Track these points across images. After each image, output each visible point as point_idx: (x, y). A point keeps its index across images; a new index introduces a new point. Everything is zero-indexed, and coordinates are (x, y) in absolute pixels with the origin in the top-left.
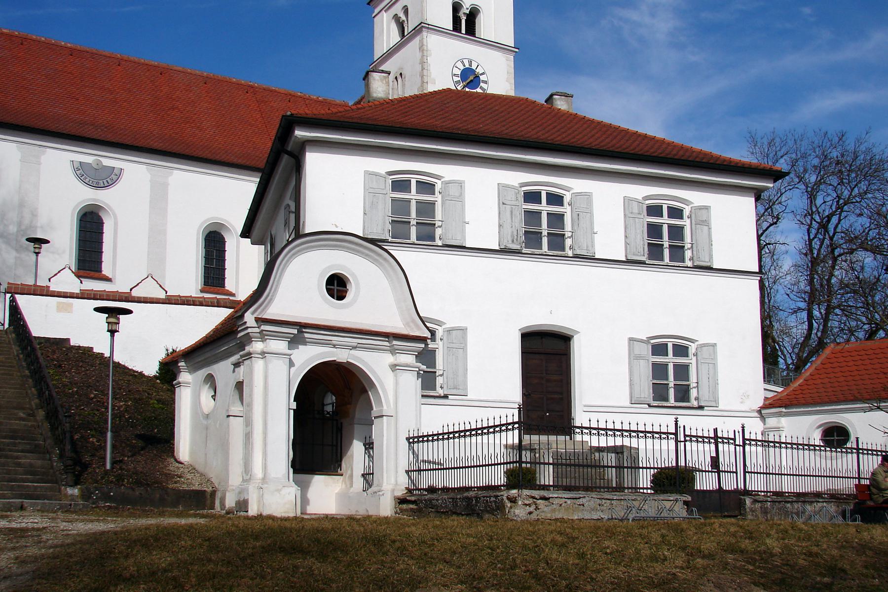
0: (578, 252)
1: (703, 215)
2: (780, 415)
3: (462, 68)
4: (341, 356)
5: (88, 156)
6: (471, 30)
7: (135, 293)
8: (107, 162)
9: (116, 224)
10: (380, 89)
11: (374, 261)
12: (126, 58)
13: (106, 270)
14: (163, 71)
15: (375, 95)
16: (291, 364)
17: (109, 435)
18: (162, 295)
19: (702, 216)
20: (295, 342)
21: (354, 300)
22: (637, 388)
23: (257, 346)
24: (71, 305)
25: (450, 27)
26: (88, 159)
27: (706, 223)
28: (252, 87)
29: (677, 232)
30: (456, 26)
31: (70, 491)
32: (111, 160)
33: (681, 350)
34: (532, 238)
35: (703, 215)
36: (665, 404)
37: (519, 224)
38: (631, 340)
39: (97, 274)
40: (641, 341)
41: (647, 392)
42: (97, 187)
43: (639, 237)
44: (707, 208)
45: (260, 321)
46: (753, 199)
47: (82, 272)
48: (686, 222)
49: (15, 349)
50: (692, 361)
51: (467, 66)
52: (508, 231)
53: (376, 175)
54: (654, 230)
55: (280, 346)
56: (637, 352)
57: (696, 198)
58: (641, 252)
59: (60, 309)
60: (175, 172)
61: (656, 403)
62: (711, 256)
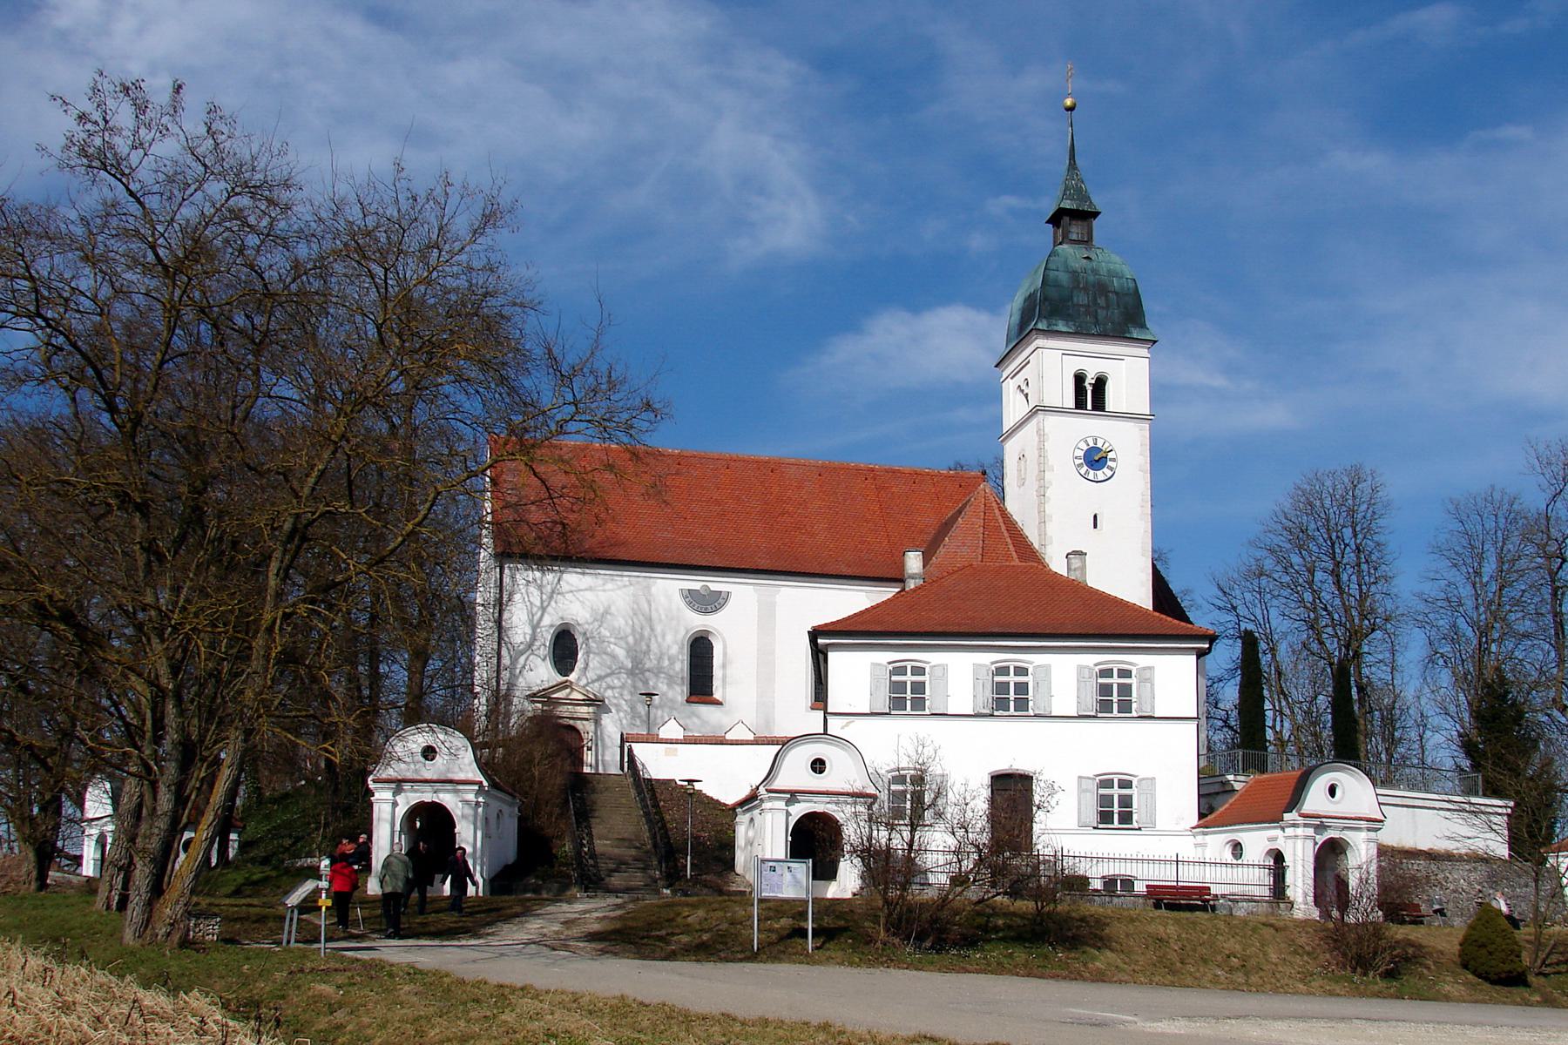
0: (1037, 712)
1: (1147, 674)
2: (1205, 834)
3: (1085, 448)
4: (819, 808)
5: (695, 582)
6: (1099, 404)
7: (728, 737)
8: (714, 587)
9: (725, 647)
10: (914, 566)
11: (843, 749)
12: (735, 457)
13: (717, 695)
14: (773, 468)
15: (910, 572)
16: (788, 814)
17: (689, 858)
18: (751, 737)
19: (1147, 676)
20: (789, 802)
21: (829, 774)
22: (1083, 817)
23: (767, 805)
24: (676, 749)
25: (1070, 402)
26: (696, 586)
27: (1150, 680)
28: (872, 470)
29: (1125, 690)
30: (1080, 403)
31: (665, 891)
32: (717, 584)
33: (1125, 784)
34: (1001, 704)
35: (1147, 674)
36: (1110, 826)
37: (988, 694)
38: (1080, 777)
39: (708, 698)
40: (1089, 778)
41: (1093, 818)
42: (706, 612)
43: (1089, 697)
44: (1151, 668)
45: (769, 791)
46: (1195, 657)
47: (694, 698)
48: (1133, 681)
49: (633, 792)
50: (1134, 792)
51: (1092, 445)
52: (980, 700)
53: (880, 665)
54: (1105, 690)
55: (781, 804)
56: (1084, 787)
57: (1139, 661)
58: (1090, 707)
59: (667, 753)
60: (783, 589)
61: (1101, 826)
62: (1153, 707)
